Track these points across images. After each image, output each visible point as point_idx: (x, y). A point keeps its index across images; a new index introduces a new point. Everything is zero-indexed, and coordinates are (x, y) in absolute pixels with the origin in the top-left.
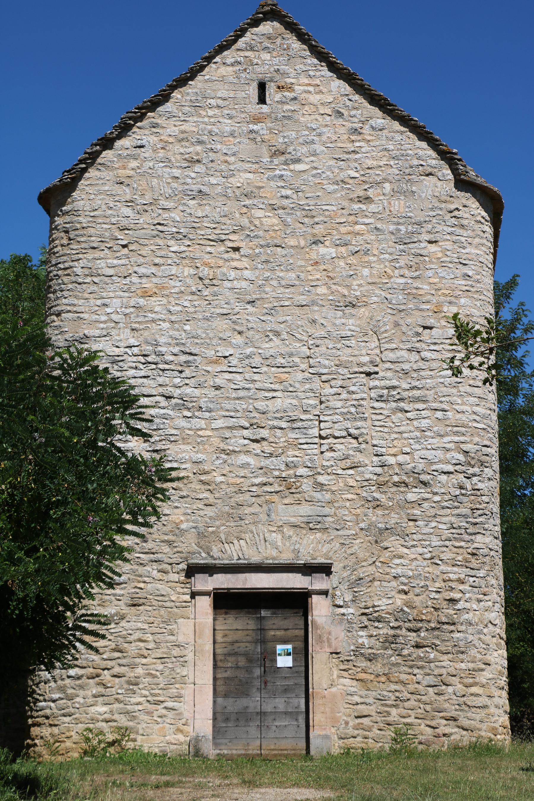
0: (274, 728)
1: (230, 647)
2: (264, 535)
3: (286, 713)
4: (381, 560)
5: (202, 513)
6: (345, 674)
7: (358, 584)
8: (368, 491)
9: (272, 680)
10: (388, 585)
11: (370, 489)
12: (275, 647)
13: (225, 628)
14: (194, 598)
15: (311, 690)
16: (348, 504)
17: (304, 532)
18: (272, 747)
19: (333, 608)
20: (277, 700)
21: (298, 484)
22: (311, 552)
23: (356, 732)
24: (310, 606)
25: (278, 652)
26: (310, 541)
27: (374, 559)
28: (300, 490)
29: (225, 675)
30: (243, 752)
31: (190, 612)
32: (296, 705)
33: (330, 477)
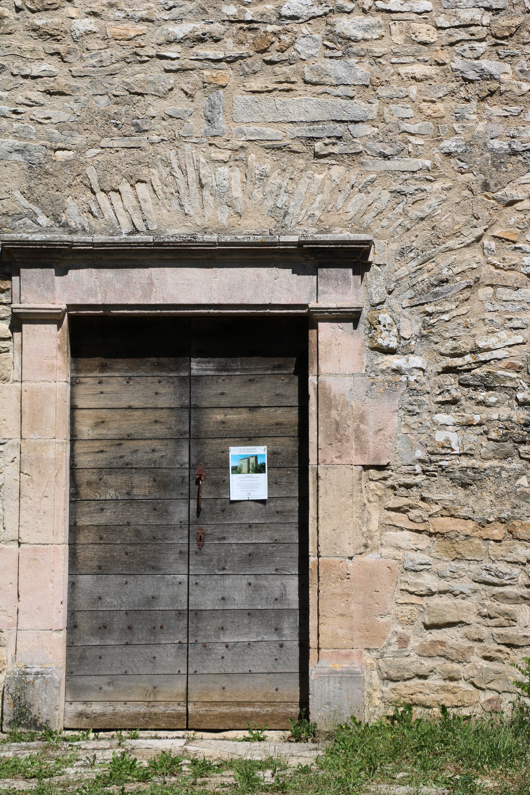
0: (221, 649)
1: (112, 452)
2: (197, 170)
3: (250, 613)
4: (497, 232)
5: (38, 113)
6: (400, 519)
7: (436, 295)
8: (468, 54)
9: (218, 533)
10: (514, 295)
11: (472, 49)
12: (226, 452)
13: (102, 404)
14: (20, 330)
15: (312, 559)
16: (413, 90)
17: (300, 162)
18: (216, 697)
19: (372, 354)
20: (228, 582)
21: (286, 39)
22: (318, 213)
23: (428, 664)
24: (312, 350)
25: (232, 463)
26: (314, 188)
27: (479, 231)
28: (290, 53)
29: (101, 519)
30: (143, 709)
31: (8, 363)
32: (277, 595)
33: (368, 20)
